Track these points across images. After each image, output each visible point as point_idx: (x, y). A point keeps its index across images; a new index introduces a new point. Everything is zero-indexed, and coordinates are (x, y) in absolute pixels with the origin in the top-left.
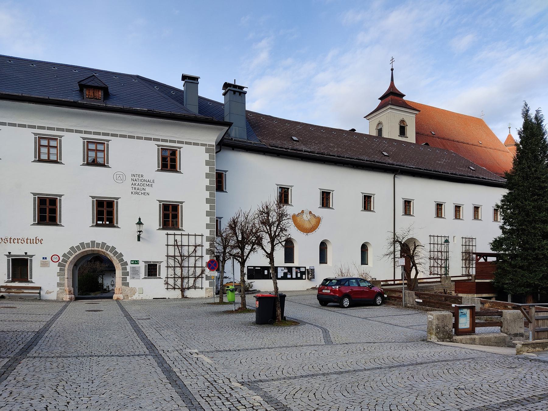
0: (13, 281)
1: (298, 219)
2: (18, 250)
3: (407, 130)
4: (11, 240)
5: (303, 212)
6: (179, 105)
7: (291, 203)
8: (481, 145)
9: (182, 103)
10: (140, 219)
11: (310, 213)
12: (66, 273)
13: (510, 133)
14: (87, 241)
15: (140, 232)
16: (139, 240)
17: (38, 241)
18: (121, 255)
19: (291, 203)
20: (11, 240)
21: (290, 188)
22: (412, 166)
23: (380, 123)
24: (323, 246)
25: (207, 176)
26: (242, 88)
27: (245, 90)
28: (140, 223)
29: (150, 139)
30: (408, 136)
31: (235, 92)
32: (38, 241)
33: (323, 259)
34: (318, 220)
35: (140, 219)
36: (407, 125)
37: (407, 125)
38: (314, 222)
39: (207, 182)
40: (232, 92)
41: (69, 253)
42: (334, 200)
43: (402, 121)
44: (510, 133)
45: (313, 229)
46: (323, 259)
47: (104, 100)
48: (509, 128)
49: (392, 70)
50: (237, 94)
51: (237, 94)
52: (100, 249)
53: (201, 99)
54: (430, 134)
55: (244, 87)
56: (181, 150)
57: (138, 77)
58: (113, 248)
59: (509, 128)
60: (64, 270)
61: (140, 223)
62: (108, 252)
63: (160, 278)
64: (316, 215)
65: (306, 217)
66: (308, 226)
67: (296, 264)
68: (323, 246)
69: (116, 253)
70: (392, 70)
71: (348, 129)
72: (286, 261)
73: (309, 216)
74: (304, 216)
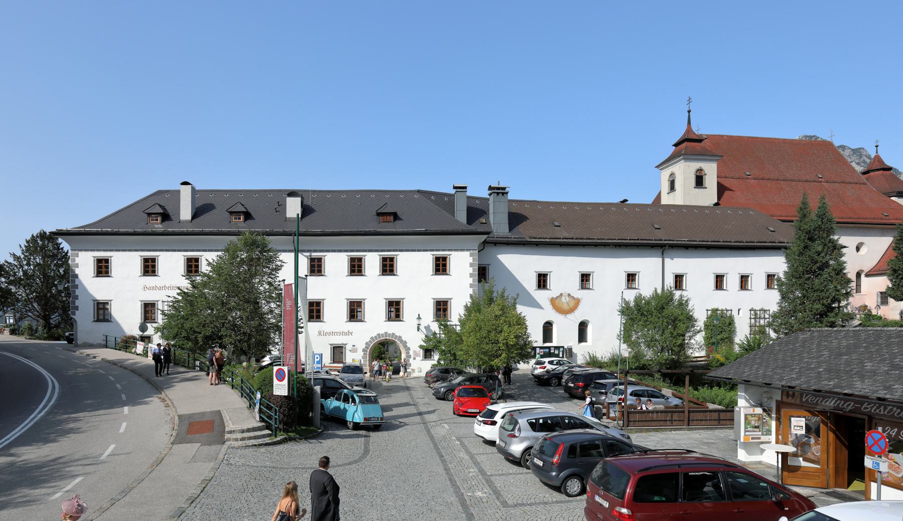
0: (334, 362)
1: (557, 302)
2: (338, 340)
3: (705, 179)
4: (333, 334)
5: (561, 295)
6: (452, 217)
7: (550, 287)
8: (820, 179)
9: (454, 215)
10: (419, 315)
11: (569, 295)
12: (368, 357)
13: (877, 152)
14: (382, 332)
15: (419, 325)
16: (418, 331)
17: (349, 333)
18: (406, 342)
19: (550, 287)
20: (333, 334)
21: (549, 274)
22: (684, 240)
23: (672, 174)
24: (583, 327)
25: (471, 265)
26: (504, 189)
27: (507, 190)
28: (419, 318)
29: (426, 250)
30: (706, 186)
31: (498, 194)
32: (349, 333)
33: (582, 337)
34: (577, 302)
35: (419, 315)
36: (705, 175)
37: (705, 175)
38: (572, 304)
39: (471, 270)
40: (496, 194)
41: (370, 341)
42: (594, 281)
43: (700, 170)
44: (877, 152)
45: (572, 310)
46: (582, 337)
47: (394, 221)
48: (877, 146)
49: (689, 112)
50: (500, 195)
51: (500, 195)
52: (391, 338)
53: (471, 199)
54: (743, 175)
55: (506, 188)
56: (451, 257)
57: (419, 191)
58: (400, 337)
59: (877, 146)
60: (366, 354)
61: (419, 318)
62: (396, 340)
63: (434, 360)
64: (575, 297)
65: (564, 299)
66: (566, 307)
67: (555, 343)
68: (583, 327)
69: (402, 340)
70: (689, 112)
71: (617, 200)
72: (545, 342)
73: (568, 299)
74: (563, 299)
